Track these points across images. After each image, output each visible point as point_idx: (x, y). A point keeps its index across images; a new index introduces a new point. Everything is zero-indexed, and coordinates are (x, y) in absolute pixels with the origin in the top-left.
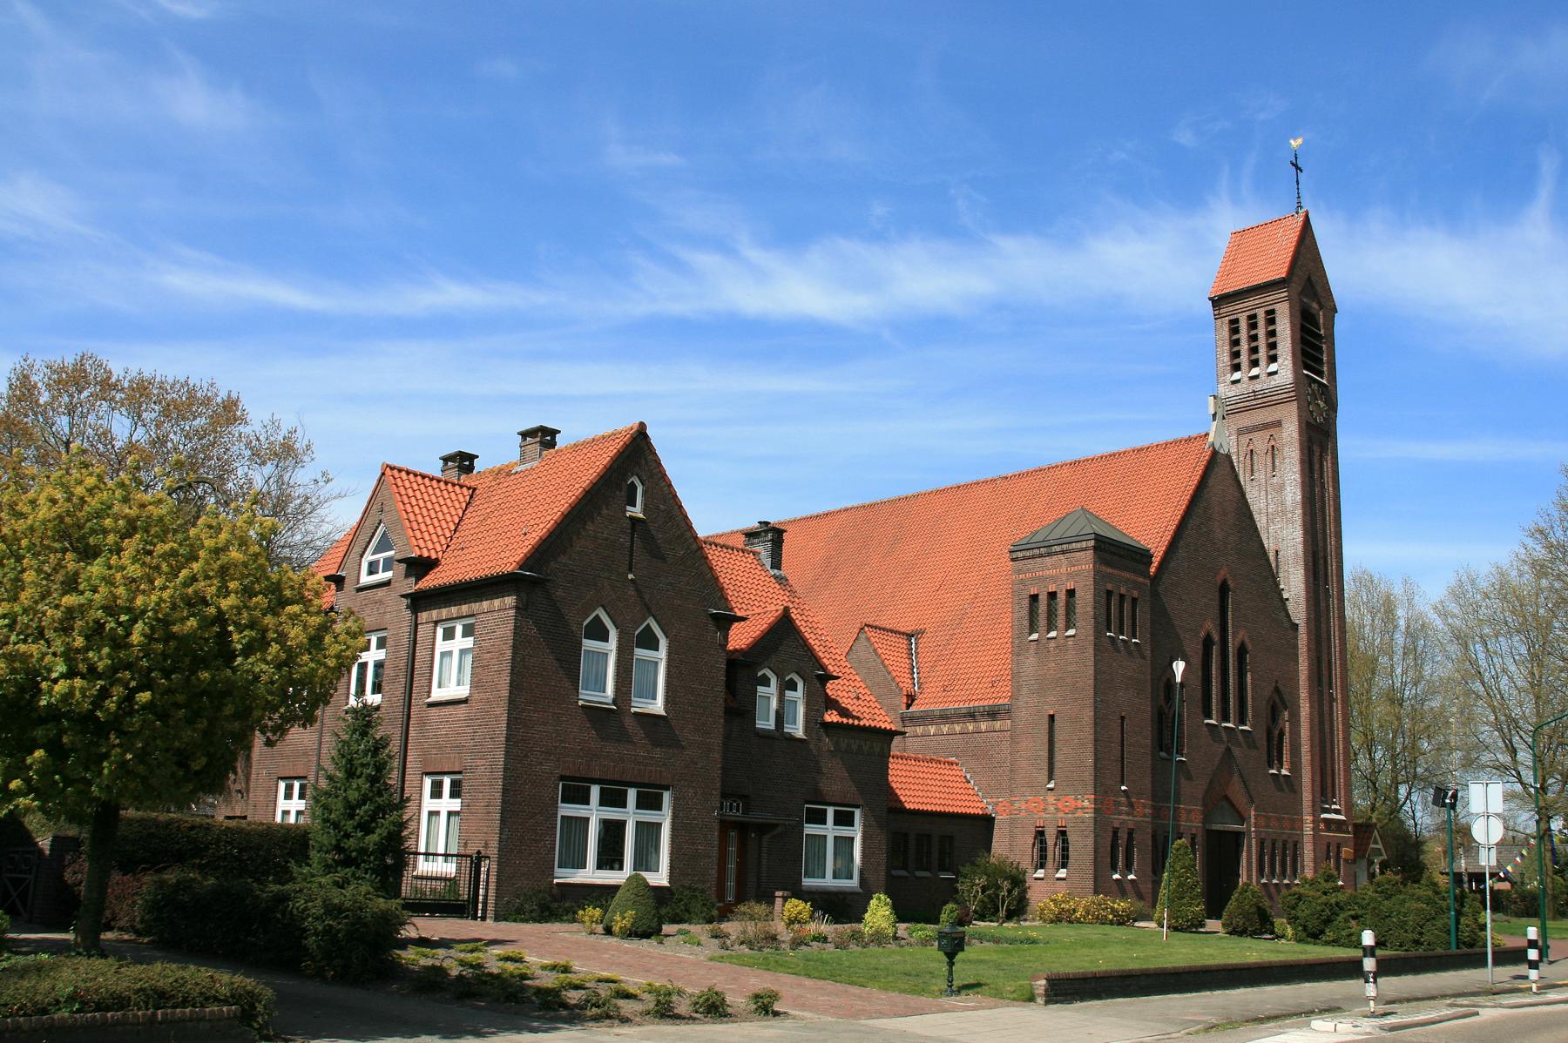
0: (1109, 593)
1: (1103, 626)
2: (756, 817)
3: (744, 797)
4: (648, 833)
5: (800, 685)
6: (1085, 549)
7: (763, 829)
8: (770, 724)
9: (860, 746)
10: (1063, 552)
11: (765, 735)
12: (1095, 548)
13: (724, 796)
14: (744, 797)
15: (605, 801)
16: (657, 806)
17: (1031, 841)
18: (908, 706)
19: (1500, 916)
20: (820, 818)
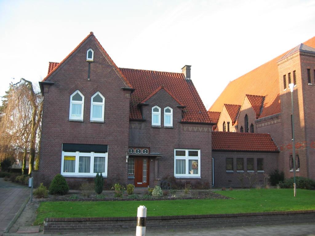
0: (309, 70)
1: (306, 80)
2: (153, 153)
3: (149, 148)
4: (134, 163)
5: (172, 110)
6: (297, 56)
7: (154, 158)
8: (81, 117)
9: (198, 129)
10: (291, 59)
11: (156, 128)
12: (301, 55)
13: (129, 147)
14: (149, 148)
15: (191, 154)
16: (196, 154)
17: (289, 159)
18: (257, 118)
19: (300, 190)
20: (183, 154)
